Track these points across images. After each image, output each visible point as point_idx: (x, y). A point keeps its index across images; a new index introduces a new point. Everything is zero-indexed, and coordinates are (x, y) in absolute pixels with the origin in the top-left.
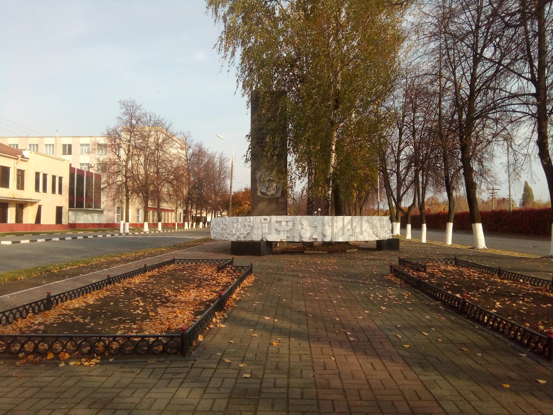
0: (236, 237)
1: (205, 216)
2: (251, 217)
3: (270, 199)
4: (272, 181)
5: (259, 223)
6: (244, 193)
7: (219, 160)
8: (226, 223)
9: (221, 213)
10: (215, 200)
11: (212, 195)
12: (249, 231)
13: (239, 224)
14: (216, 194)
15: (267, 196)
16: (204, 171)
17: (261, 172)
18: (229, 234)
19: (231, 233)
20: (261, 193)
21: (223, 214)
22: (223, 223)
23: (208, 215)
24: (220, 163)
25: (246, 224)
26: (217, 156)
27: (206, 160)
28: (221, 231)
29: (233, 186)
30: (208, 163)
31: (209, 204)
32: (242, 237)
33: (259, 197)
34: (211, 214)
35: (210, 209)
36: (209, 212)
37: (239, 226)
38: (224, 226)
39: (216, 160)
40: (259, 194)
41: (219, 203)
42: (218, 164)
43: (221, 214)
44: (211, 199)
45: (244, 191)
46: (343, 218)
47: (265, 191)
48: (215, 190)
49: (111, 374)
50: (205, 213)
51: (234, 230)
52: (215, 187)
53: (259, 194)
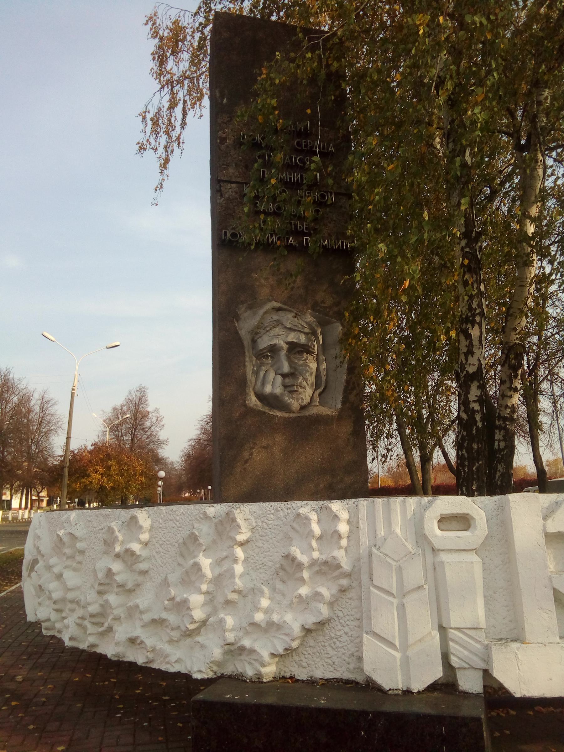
0: (217, 653)
1: (9, 498)
2: (336, 506)
3: (298, 420)
4: (305, 349)
5: (410, 546)
6: (90, 452)
7: (39, 402)
8: (136, 547)
9: (39, 493)
10: (29, 470)
11: (23, 462)
12: (325, 611)
13: (239, 552)
14: (30, 458)
15: (286, 408)
16: (11, 417)
17: (261, 312)
18: (158, 622)
19: (172, 618)
20: (261, 397)
21: (41, 494)
22: (109, 543)
23: (14, 497)
24: (42, 408)
25: (303, 559)
26: (36, 396)
27: (15, 399)
28: (91, 596)
29: (72, 435)
30: (18, 405)
31: (18, 478)
32: (265, 654)
33: (250, 411)
34: (19, 495)
35: (19, 486)
36: (16, 492)
37: (239, 569)
38: (116, 567)
39: (32, 403)
40: (253, 401)
41: (36, 476)
42: (37, 409)
43: (38, 496)
44: (20, 468)
45: (92, 448)
46: (404, 502)
47: (278, 390)
48: (29, 453)
49: (229, 186)
50: (8, 493)
51: (196, 599)
52: (29, 447)
53: (253, 401)
